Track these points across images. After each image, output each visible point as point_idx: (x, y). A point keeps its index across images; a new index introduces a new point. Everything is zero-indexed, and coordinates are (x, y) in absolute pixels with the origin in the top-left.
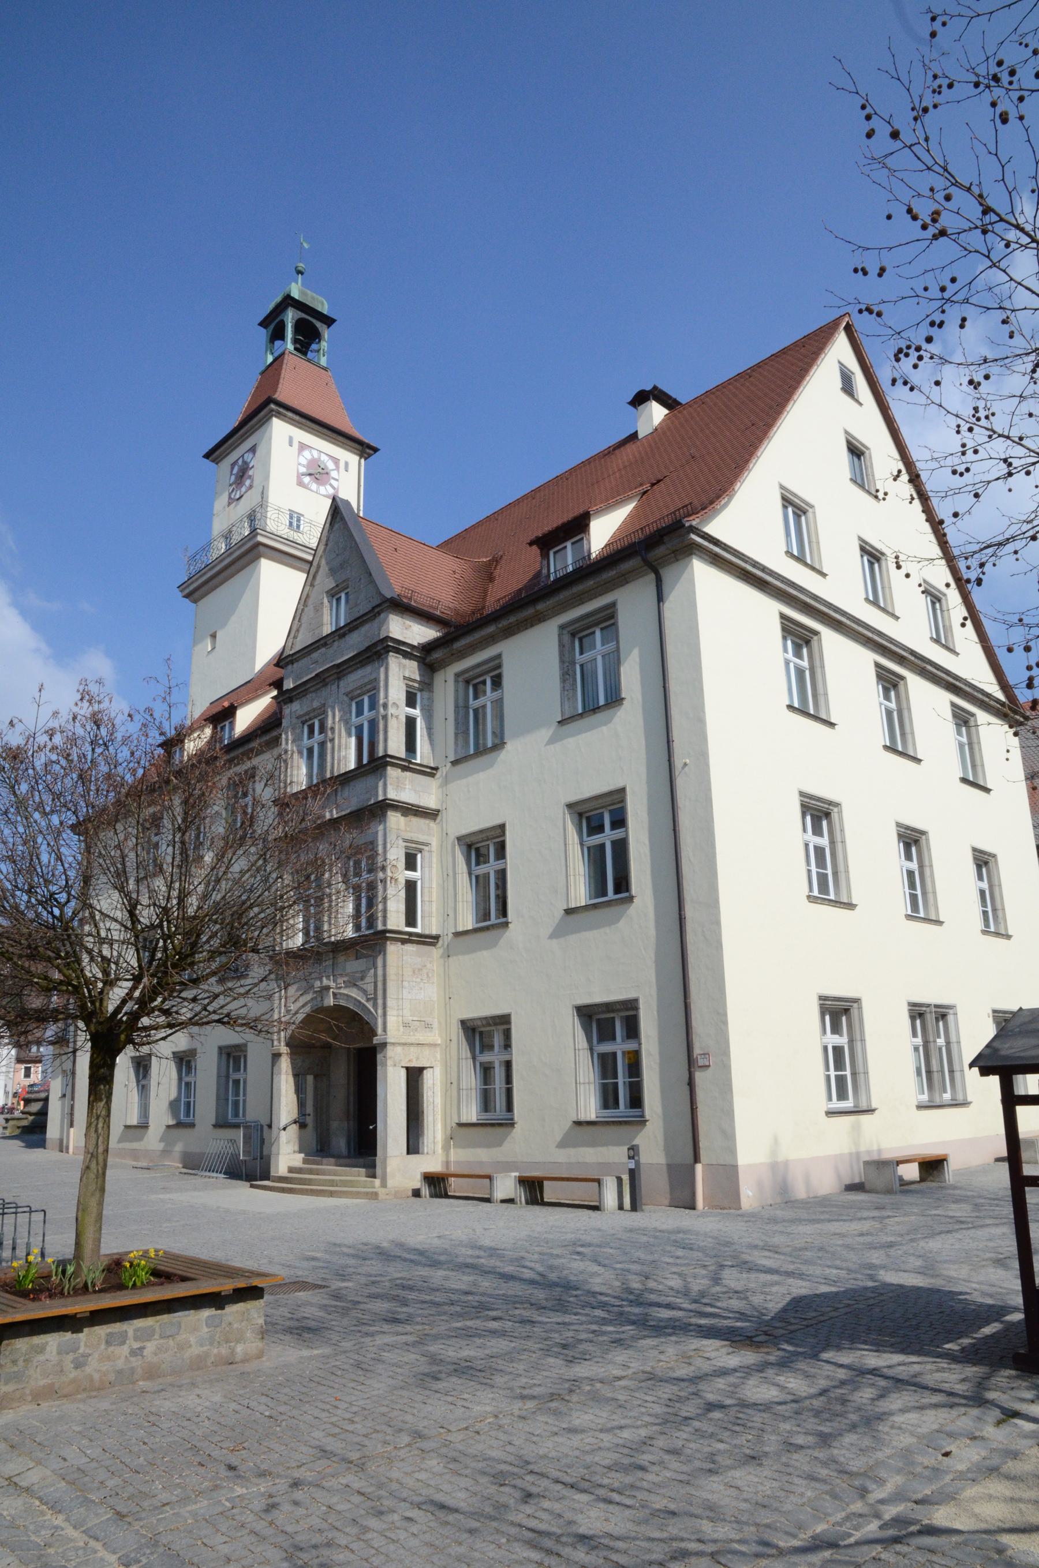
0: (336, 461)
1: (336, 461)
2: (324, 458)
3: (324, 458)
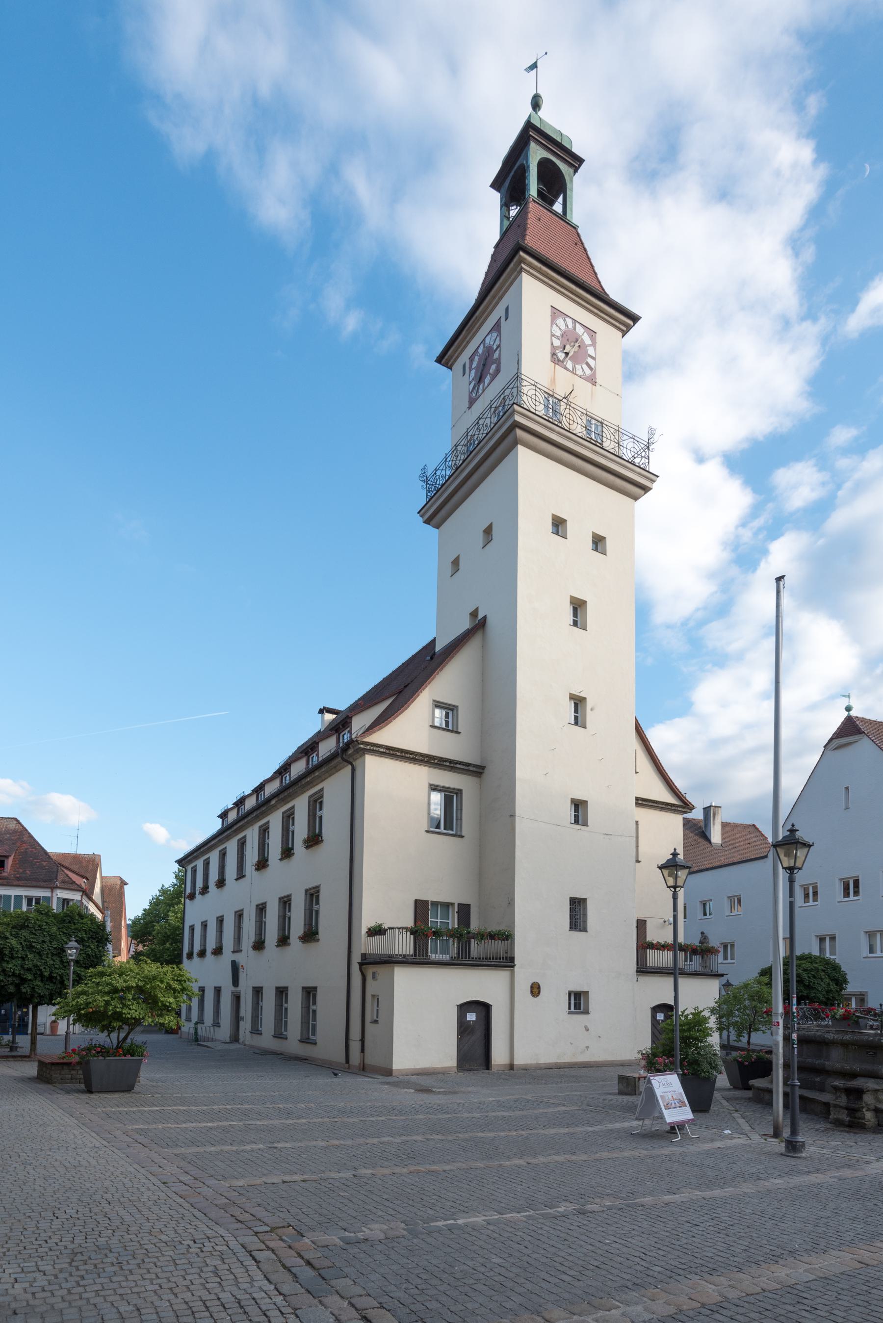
0: (592, 333)
1: (592, 333)
2: (580, 330)
3: (580, 330)
